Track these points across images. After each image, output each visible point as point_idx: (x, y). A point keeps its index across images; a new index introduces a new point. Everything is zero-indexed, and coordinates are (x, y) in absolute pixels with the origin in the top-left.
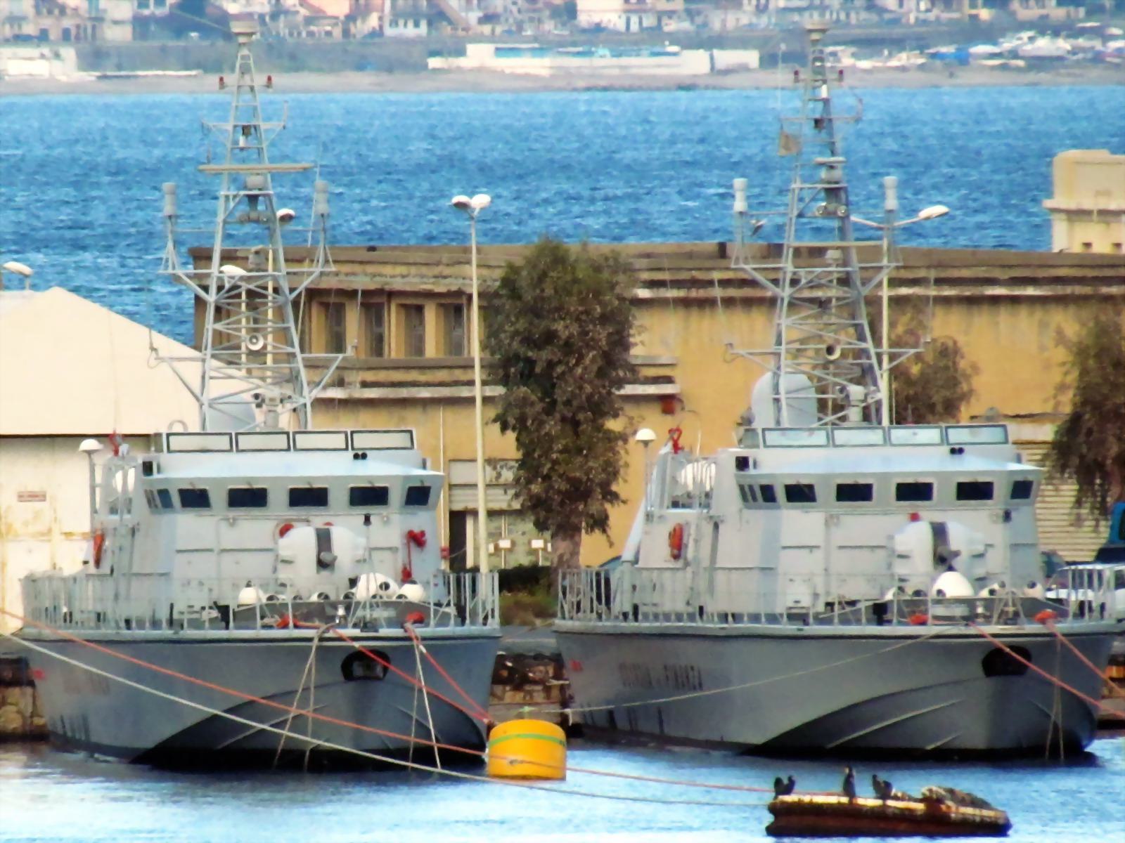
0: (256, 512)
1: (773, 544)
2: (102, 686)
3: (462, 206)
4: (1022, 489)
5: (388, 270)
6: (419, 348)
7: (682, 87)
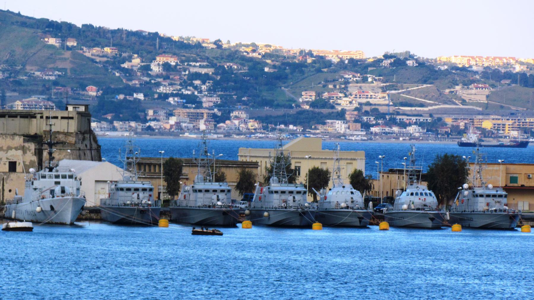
0: (284, 194)
1: (196, 197)
2: (109, 214)
3: (160, 153)
4: (229, 191)
5: (152, 161)
6: (155, 171)
7: (213, 140)
